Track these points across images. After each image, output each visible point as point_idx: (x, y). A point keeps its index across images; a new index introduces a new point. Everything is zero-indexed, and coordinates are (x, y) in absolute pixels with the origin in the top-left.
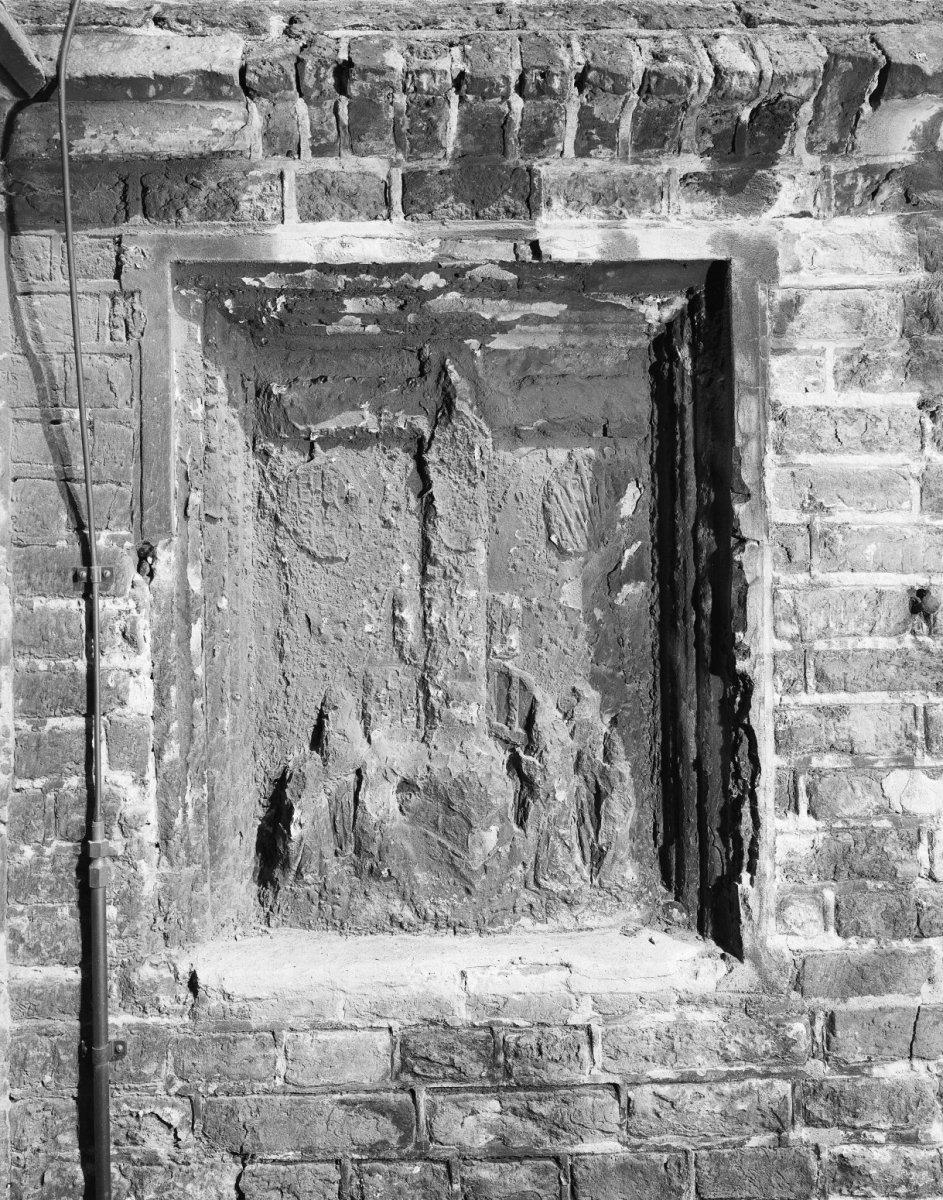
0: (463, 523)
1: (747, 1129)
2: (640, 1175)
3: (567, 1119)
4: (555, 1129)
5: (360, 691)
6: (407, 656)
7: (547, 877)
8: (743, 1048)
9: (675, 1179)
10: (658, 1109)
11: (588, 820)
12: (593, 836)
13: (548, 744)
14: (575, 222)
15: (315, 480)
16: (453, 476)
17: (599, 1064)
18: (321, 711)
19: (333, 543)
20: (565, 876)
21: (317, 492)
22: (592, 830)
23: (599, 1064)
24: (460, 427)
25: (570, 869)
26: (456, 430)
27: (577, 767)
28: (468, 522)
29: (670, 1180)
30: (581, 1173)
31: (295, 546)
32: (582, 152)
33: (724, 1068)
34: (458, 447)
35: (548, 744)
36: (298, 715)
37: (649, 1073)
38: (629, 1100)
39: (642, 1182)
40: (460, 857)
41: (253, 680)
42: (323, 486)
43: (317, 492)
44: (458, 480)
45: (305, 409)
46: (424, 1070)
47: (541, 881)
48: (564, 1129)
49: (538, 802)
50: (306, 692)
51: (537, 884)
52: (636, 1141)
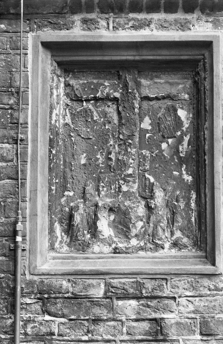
0: (131, 127)
1: (216, 312)
2: (182, 325)
3: (159, 307)
4: (156, 310)
5: (97, 181)
6: (112, 170)
7: (156, 239)
8: (215, 286)
9: (193, 327)
10: (188, 304)
11: (170, 222)
12: (172, 227)
13: (157, 196)
14: (214, 31)
15: (83, 113)
16: (128, 112)
17: (169, 290)
18: (84, 188)
19: (89, 133)
20: (162, 239)
21: (84, 117)
22: (171, 226)
23: (169, 290)
24: (130, 96)
25: (163, 237)
26: (129, 97)
27: (167, 206)
28: (133, 127)
29: (191, 327)
30: (163, 325)
31: (76, 134)
32: (28, 88)
33: (209, 293)
34: (129, 102)
35: (157, 196)
36: (76, 189)
37: (185, 293)
38: (179, 301)
39: (182, 328)
40: (128, 232)
41: (62, 177)
42: (86, 115)
43: (84, 117)
44: (130, 113)
45: (81, 90)
46: (115, 291)
47: (154, 240)
48: (158, 310)
49: (154, 215)
50: (79, 182)
51: (153, 241)
52: (181, 315)
